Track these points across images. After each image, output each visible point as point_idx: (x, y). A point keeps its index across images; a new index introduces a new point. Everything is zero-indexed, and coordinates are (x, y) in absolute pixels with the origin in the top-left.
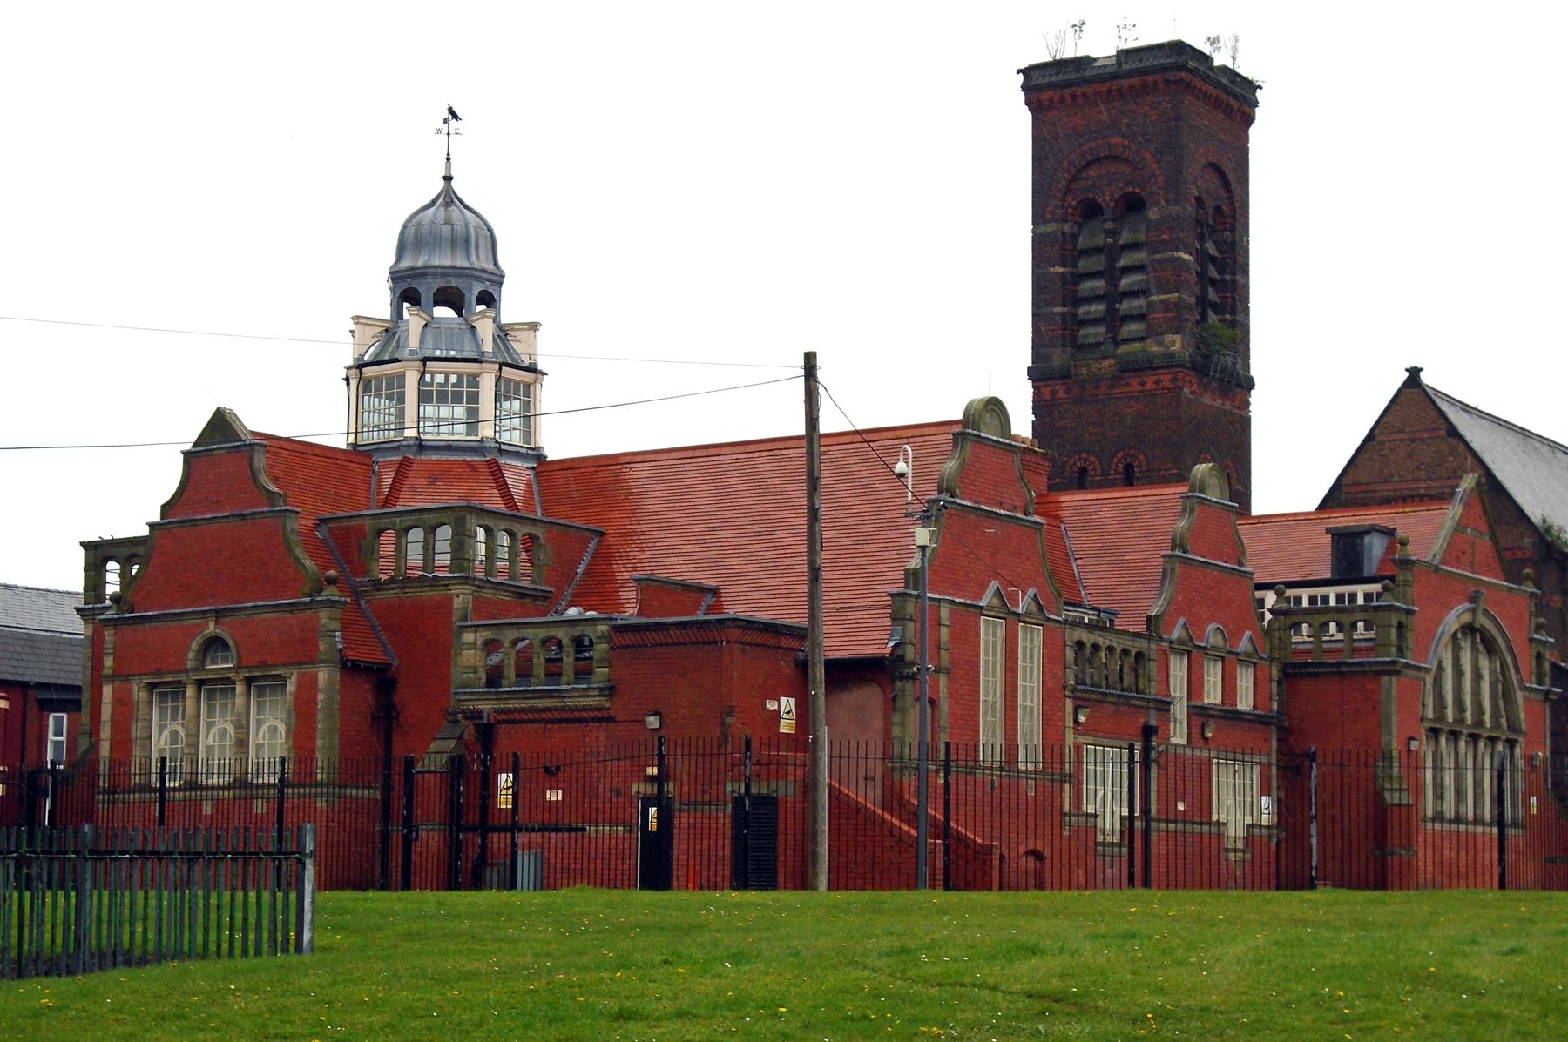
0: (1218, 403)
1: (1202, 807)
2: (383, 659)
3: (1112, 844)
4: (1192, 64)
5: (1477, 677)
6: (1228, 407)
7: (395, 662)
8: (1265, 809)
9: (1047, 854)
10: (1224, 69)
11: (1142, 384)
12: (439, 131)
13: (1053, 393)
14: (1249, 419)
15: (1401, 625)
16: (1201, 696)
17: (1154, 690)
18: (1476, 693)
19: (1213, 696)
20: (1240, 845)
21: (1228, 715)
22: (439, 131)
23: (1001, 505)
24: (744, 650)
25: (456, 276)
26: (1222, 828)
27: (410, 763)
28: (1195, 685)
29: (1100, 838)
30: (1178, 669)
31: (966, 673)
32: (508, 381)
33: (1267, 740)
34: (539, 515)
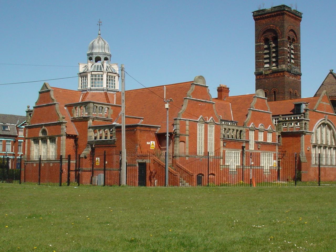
0: (294, 78)
1: (258, 163)
2: (76, 134)
3: (235, 172)
4: (286, 9)
5: (327, 134)
6: (296, 79)
7: (78, 135)
8: (274, 163)
9: (205, 174)
10: (294, 10)
11: (277, 75)
12: (98, 25)
13: (259, 77)
14: (300, 82)
15: (305, 124)
16: (258, 139)
17: (244, 138)
18: (326, 138)
19: (261, 139)
20: (269, 171)
21: (265, 144)
22: (98, 25)
23: (203, 99)
24: (141, 131)
25: (99, 54)
26: (263, 168)
27: (79, 155)
28: (256, 137)
29: (230, 170)
30: (252, 134)
31: (193, 136)
32: (110, 76)
33: (275, 148)
34: (115, 104)
